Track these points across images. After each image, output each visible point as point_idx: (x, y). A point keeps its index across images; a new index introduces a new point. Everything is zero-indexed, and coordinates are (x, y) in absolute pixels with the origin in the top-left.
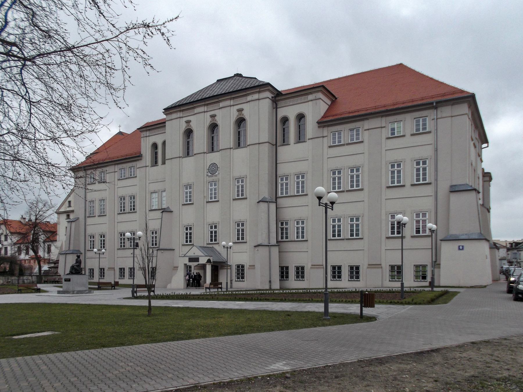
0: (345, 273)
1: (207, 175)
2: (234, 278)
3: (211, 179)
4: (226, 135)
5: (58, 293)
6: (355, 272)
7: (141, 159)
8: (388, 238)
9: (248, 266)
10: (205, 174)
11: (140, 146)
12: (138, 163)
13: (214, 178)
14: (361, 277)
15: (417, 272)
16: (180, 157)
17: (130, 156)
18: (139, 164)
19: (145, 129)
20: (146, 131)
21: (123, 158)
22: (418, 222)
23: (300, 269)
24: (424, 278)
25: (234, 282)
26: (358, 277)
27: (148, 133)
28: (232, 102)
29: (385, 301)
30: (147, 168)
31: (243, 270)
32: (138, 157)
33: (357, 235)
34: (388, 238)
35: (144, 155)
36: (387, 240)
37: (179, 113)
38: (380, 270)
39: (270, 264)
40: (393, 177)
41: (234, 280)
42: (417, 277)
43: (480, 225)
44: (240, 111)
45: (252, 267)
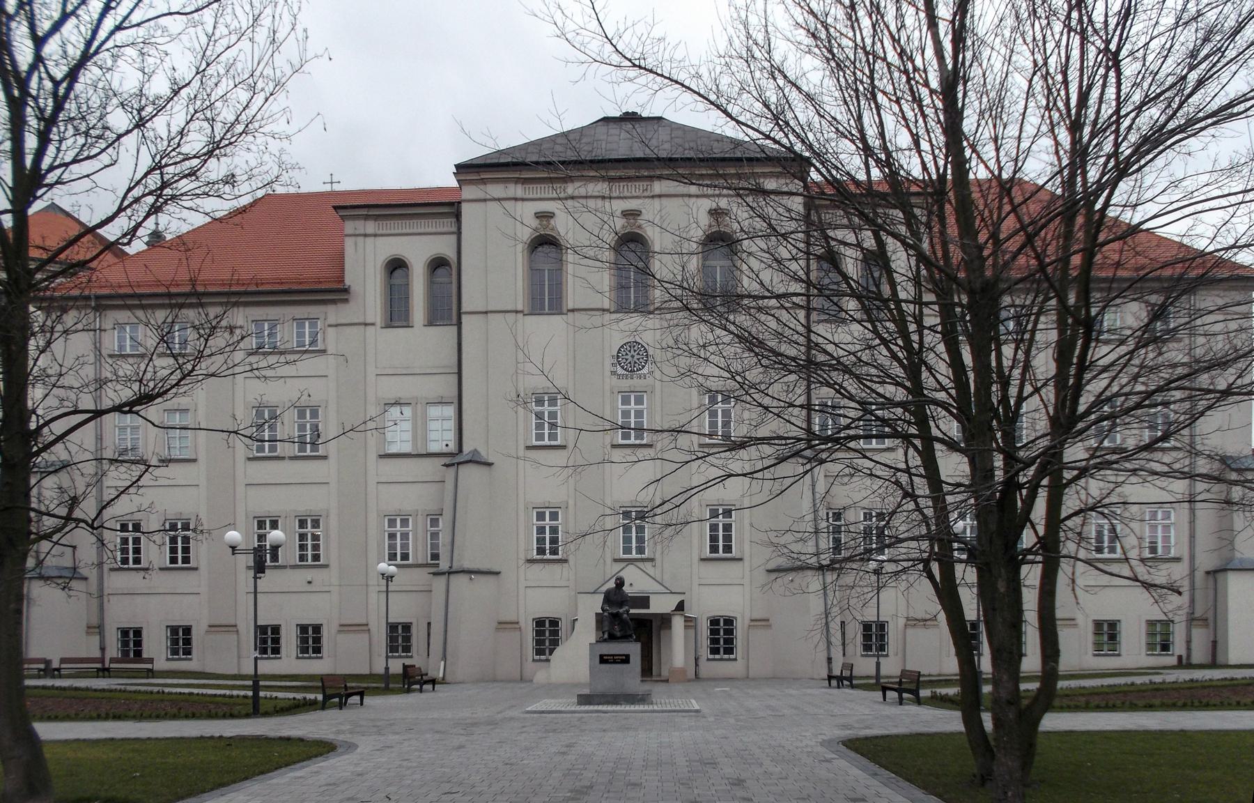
0: (289, 640)
1: (613, 373)
2: (705, 652)
3: (626, 384)
5: (580, 703)
6: (311, 639)
7: (346, 301)
9: (747, 622)
10: (608, 368)
12: (331, 309)
13: (636, 383)
14: (194, 651)
15: (1151, 634)
16: (517, 312)
17: (295, 287)
18: (332, 313)
20: (367, 217)
21: (285, 287)
22: (392, 536)
23: (131, 635)
24: (1165, 647)
26: (317, 650)
27: (371, 227)
28: (518, 190)
29: (1118, 703)
30: (370, 329)
31: (729, 632)
32: (333, 291)
33: (728, 549)
38: (366, 636)
42: (1151, 646)
43: (1192, 536)
45: (761, 623)
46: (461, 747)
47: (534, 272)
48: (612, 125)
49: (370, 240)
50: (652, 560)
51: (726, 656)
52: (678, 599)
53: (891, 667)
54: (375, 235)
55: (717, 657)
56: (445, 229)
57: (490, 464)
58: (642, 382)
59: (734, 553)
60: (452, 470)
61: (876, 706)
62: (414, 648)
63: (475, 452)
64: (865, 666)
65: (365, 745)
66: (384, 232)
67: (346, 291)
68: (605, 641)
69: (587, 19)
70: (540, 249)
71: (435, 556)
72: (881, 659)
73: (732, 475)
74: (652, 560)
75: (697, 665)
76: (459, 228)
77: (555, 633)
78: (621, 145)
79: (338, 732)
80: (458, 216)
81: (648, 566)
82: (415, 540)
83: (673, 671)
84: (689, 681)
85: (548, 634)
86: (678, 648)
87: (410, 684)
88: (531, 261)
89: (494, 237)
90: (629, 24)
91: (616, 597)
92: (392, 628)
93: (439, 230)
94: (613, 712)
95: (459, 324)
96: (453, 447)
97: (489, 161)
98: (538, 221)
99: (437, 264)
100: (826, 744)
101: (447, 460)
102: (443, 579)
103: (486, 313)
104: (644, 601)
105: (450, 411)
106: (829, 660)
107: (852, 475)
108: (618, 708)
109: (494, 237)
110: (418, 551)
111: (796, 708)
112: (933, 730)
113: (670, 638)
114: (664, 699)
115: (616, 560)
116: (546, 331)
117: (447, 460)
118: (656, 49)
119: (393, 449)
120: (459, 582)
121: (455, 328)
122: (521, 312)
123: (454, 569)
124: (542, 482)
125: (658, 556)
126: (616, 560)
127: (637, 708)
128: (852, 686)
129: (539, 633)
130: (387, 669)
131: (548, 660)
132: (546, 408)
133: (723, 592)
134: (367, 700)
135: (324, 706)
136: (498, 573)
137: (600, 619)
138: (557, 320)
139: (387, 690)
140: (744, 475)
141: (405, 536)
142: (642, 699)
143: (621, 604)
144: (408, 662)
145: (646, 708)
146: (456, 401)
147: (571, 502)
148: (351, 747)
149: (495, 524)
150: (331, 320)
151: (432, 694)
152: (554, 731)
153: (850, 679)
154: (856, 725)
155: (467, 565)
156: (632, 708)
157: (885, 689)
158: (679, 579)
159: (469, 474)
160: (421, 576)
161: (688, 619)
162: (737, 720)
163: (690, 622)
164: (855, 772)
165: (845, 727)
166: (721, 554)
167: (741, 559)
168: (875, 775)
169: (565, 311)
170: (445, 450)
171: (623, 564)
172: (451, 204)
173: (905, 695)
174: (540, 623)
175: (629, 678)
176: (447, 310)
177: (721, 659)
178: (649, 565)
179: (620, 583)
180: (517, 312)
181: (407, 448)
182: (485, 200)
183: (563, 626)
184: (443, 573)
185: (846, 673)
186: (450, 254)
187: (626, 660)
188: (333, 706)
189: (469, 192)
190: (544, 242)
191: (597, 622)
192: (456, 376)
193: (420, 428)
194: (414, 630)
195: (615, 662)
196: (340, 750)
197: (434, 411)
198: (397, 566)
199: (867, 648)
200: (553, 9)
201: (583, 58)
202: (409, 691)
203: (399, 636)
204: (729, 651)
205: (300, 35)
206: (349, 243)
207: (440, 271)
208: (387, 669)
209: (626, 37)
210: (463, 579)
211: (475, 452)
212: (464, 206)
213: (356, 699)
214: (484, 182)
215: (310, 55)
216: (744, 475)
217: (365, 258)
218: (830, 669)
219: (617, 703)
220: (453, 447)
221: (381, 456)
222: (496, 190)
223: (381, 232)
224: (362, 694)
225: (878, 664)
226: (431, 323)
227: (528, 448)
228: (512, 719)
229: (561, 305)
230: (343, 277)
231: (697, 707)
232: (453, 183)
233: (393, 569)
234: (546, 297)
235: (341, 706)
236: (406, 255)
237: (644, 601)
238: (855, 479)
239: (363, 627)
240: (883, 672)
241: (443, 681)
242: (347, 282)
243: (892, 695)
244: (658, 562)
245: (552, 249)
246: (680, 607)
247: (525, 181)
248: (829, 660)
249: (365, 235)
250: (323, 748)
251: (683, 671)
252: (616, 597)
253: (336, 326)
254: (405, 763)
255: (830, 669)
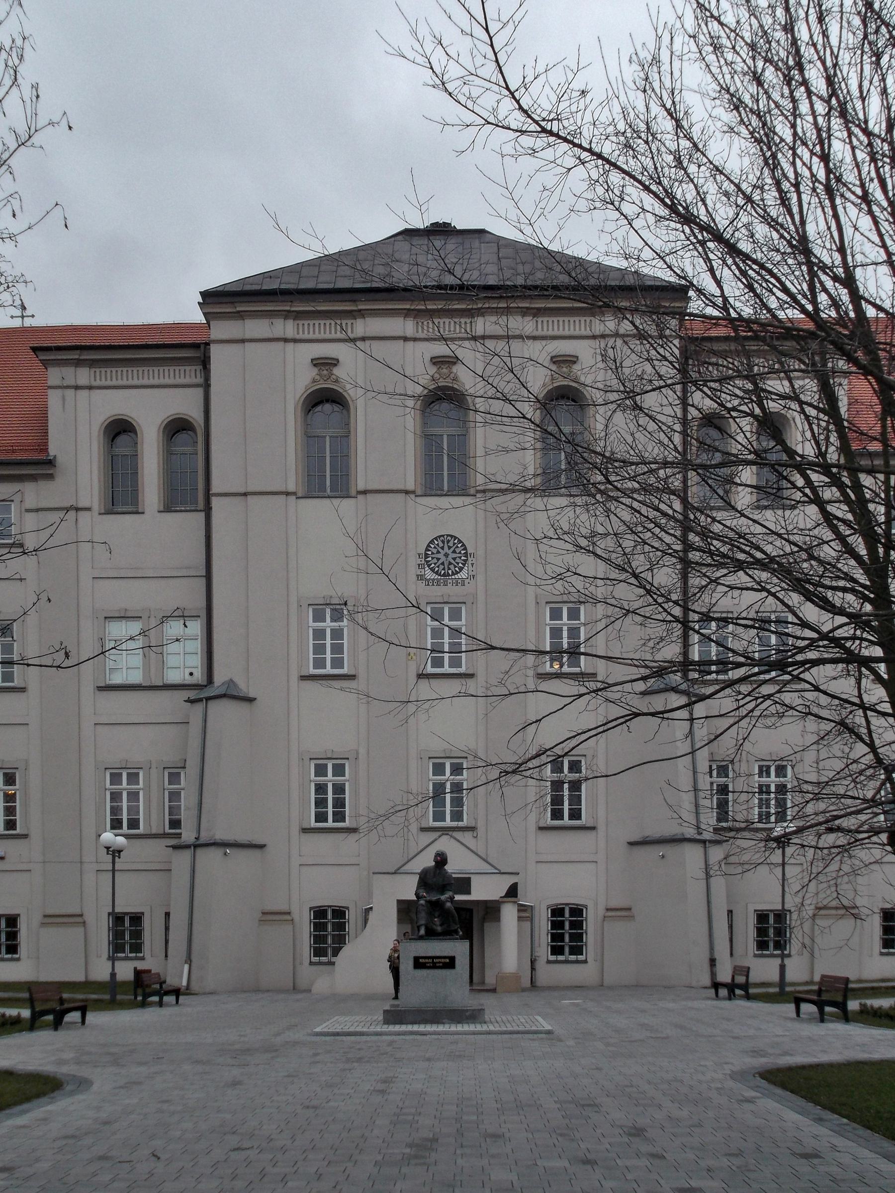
2: (543, 950)
3: (437, 592)
4: (387, 441)
5: (387, 1022)
7: (51, 477)
8: (305, 830)
9: (601, 912)
10: (413, 571)
11: (40, 421)
13: (450, 591)
16: (287, 494)
18: (33, 494)
19: (75, 355)
20: (78, 363)
22: (116, 797)
25: (541, 964)
27: (84, 376)
28: (289, 328)
30: (84, 516)
31: (577, 925)
34: (305, 830)
35: (62, 460)
36: (540, 832)
37: (279, 323)
38: (81, 930)
39: (709, 902)
40: (319, 649)
41: (306, 962)
44: (325, 364)
45: (623, 913)
46: (235, 1084)
47: (310, 439)
48: (416, 241)
49: (84, 393)
50: (472, 829)
51: (573, 958)
52: (509, 881)
53: (797, 971)
54: (90, 388)
55: (561, 958)
56: (187, 381)
57: (251, 700)
58: (458, 589)
59: (584, 820)
60: (199, 708)
61: (789, 1024)
62: (146, 947)
63: (231, 683)
64: (765, 970)
65: (103, 1080)
66: (104, 383)
67: (51, 463)
68: (421, 938)
69: (479, 60)
70: (319, 408)
71: (175, 824)
72: (787, 961)
73: (636, 715)
74: (472, 829)
75: (533, 969)
76: (207, 379)
77: (340, 927)
78: (427, 268)
79: (61, 1062)
80: (205, 363)
81: (467, 837)
82: (148, 801)
83: (502, 977)
84: (524, 990)
85: (330, 929)
86: (510, 945)
87: (146, 996)
88: (306, 424)
89: (259, 386)
90: (541, 68)
91: (436, 879)
92: (118, 919)
93: (179, 381)
94: (435, 1033)
95: (208, 510)
96: (199, 676)
97: (248, 288)
98: (315, 371)
99: (177, 428)
100: (739, 1076)
101: (192, 694)
102: (187, 854)
103: (245, 494)
104: (464, 885)
105: (196, 627)
106: (713, 962)
107: (781, 716)
108: (440, 1028)
109: (259, 386)
110: (152, 818)
111: (682, 1027)
112: (876, 1056)
113: (498, 930)
114: (503, 1015)
115: (423, 830)
116: (324, 519)
117: (192, 694)
118: (574, 108)
119: (117, 679)
120: (209, 859)
121: (202, 515)
122: (294, 494)
123: (202, 841)
124: (328, 722)
125: (481, 825)
126: (423, 830)
127: (466, 1028)
128: (748, 997)
129: (319, 927)
130: (113, 975)
131: (333, 964)
132: (328, 624)
133: (565, 872)
134: (91, 1017)
135: (32, 1025)
136: (262, 847)
137: (405, 909)
138: (346, 505)
139: (113, 1004)
140: (653, 714)
141: (133, 796)
142: (474, 1016)
143: (443, 889)
144: (141, 965)
145: (479, 1028)
146: (203, 614)
147: (362, 751)
148: (83, 1084)
149: (256, 780)
150: (30, 503)
151: (176, 1008)
152: (359, 1060)
153: (745, 987)
154: (770, 1051)
155: (220, 835)
156: (459, 1028)
157: (798, 1001)
158: (514, 856)
159: (223, 713)
160: (156, 850)
161: (522, 908)
162: (608, 1045)
163: (525, 913)
164: (791, 1116)
165: (756, 1053)
166: (566, 821)
167: (593, 828)
168: (819, 1120)
169: (353, 493)
170: (189, 680)
171: (434, 835)
172: (195, 346)
173: (828, 1009)
174: (319, 913)
175: (453, 988)
176: (190, 491)
177: (566, 962)
178: (468, 835)
179: (441, 860)
180: (287, 494)
181: (136, 677)
182: (243, 341)
183: (353, 918)
184: (187, 847)
185: (741, 979)
186: (195, 414)
187: (450, 963)
188: (45, 1026)
189: (221, 330)
190: (325, 399)
191: (399, 911)
192: (203, 581)
193: (153, 649)
194: (146, 922)
195: (434, 966)
196: (69, 1088)
197: (174, 628)
198: (127, 836)
199: (762, 945)
200: (429, 46)
201: (469, 117)
202: (144, 1004)
203: (126, 931)
204: (577, 950)
205: (27, 92)
206: (54, 399)
207: (182, 437)
208: (113, 975)
209: (535, 89)
210: (215, 854)
211: (231, 683)
212: (214, 349)
213: (75, 1016)
214: (240, 316)
215: (41, 122)
216: (653, 714)
217: (75, 418)
218: (713, 974)
219: (438, 1022)
220: (199, 676)
221: (101, 689)
222: (255, 328)
223: (98, 383)
224: (83, 1010)
225: (782, 968)
226: (168, 507)
227: (304, 678)
228: (296, 1043)
229: (348, 483)
230: (46, 444)
231: (548, 1027)
232: (197, 317)
233: (121, 840)
234: (328, 474)
235: (57, 1024)
236: (108, 415)
237: (464, 885)
238: (785, 720)
239: (76, 919)
240: (790, 976)
241: (188, 991)
242: (52, 451)
243: (807, 1008)
244: (481, 831)
245: (336, 408)
246: (513, 892)
247: (298, 316)
248: (713, 962)
249: (77, 388)
250: (41, 1086)
251: (516, 977)
252: (436, 879)
253: (37, 510)
254: (165, 1106)
255: (713, 974)
